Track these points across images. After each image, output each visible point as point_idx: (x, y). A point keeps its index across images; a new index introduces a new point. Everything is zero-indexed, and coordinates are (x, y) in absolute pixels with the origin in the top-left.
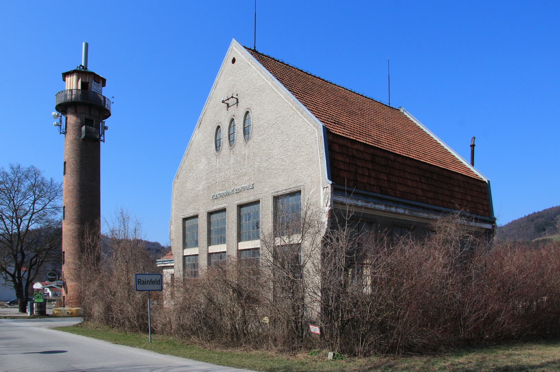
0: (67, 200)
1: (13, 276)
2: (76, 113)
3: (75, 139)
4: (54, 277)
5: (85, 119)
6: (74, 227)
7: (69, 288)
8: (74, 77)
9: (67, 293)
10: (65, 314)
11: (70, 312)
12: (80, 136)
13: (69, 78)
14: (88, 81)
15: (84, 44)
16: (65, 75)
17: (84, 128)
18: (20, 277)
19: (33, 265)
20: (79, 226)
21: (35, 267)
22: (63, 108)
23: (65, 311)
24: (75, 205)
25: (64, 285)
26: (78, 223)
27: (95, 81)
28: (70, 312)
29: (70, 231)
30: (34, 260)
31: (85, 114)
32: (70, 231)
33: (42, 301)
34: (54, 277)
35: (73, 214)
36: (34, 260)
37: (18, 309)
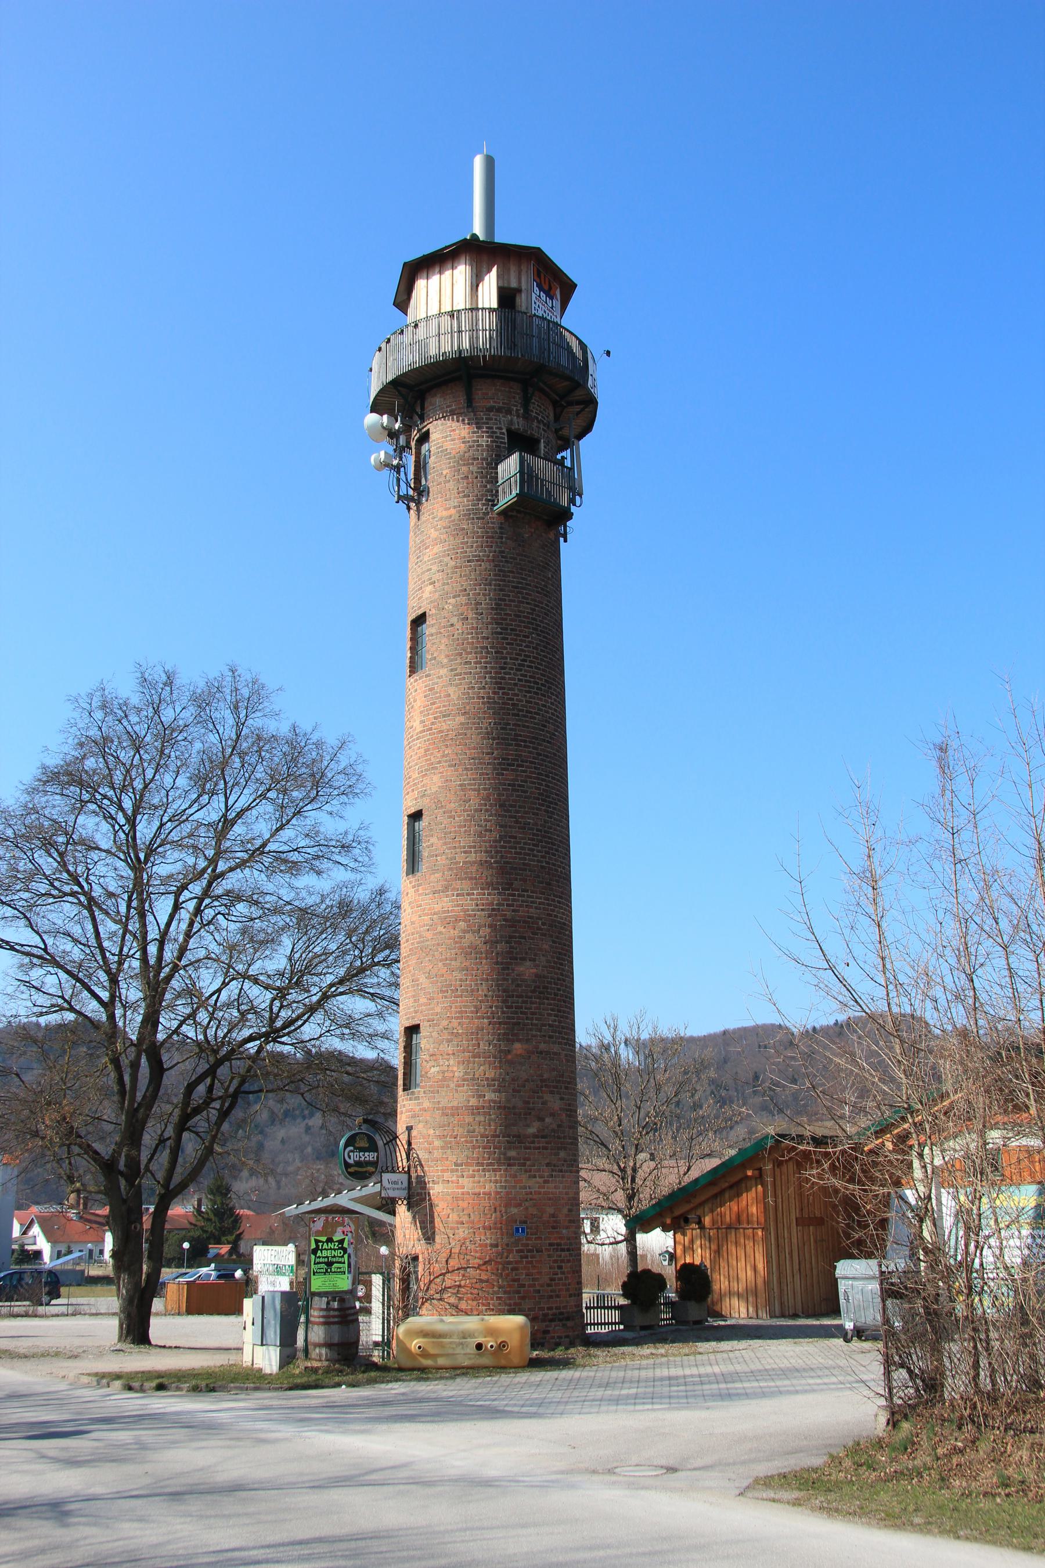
0: (434, 782)
1: (108, 1167)
2: (469, 410)
3: (469, 515)
4: (370, 1156)
5: (509, 431)
6: (469, 903)
7: (442, 1209)
8: (461, 272)
9: (429, 1237)
10: (466, 1356)
11: (490, 1343)
12: (493, 502)
13: (435, 279)
14: (514, 284)
15: (478, 162)
16: (415, 270)
17: (510, 466)
18: (134, 1171)
19: (197, 1111)
20: (496, 899)
21: (199, 1122)
22: (410, 397)
23: (465, 1335)
24: (475, 802)
25: (417, 1197)
26: (490, 885)
27: (541, 289)
28: (490, 1343)
29: (450, 922)
30: (201, 1089)
31: (509, 412)
32: (450, 922)
33: (343, 1283)
34: (370, 1156)
35: (465, 841)
36: (201, 1089)
37: (115, 1322)
